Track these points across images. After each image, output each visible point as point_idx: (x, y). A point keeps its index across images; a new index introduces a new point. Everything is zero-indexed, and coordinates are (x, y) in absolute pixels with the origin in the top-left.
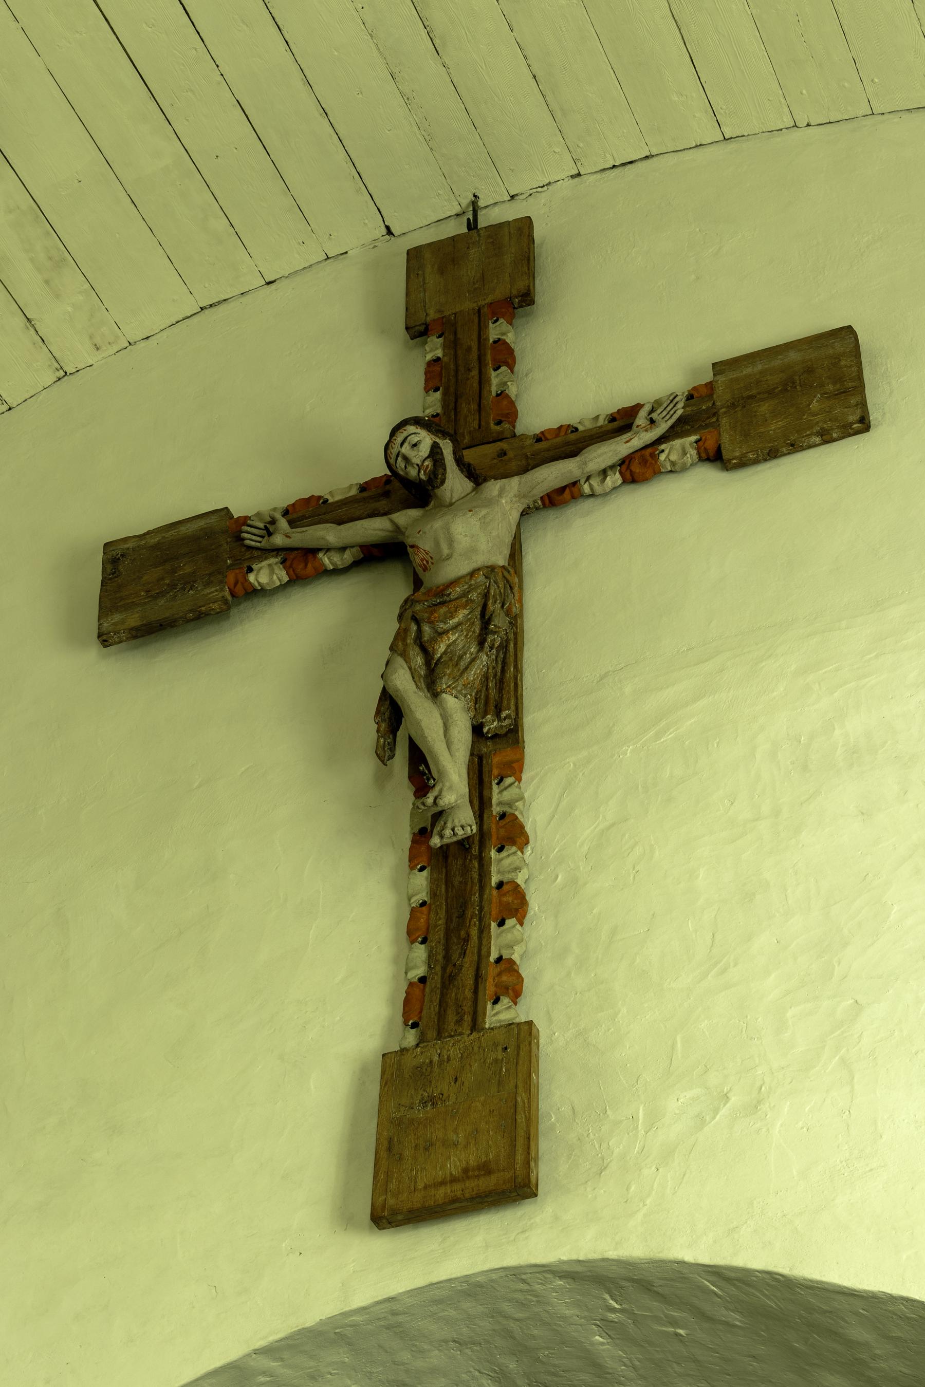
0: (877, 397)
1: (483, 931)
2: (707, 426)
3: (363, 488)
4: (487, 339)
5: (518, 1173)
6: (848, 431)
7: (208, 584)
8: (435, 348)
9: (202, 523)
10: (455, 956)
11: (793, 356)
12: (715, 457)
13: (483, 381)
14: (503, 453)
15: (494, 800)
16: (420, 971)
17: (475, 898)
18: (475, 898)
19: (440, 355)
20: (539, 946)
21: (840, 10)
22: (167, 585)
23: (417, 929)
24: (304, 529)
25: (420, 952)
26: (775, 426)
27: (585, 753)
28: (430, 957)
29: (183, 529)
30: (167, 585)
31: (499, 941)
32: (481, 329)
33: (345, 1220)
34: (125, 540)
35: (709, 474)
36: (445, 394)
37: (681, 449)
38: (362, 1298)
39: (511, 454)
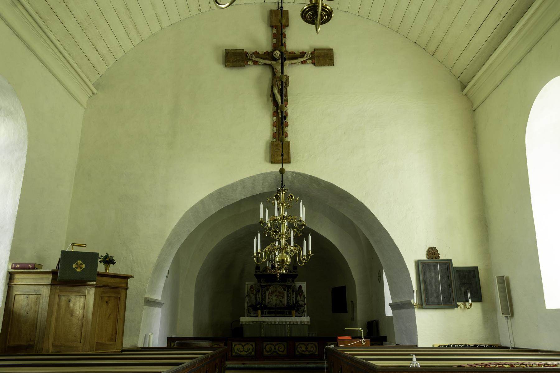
0: (336, 61)
3: (265, 53)
6: (331, 65)
11: (325, 51)
12: (314, 64)
16: (275, 131)
20: (289, 130)
21: (58, 83)
22: (235, 58)
23: (274, 125)
24: (76, 249)
25: (275, 128)
26: (322, 62)
27: (270, 283)
29: (238, 51)
30: (235, 58)
33: (266, 161)
35: (312, 66)
37: (309, 61)
38: (268, 171)
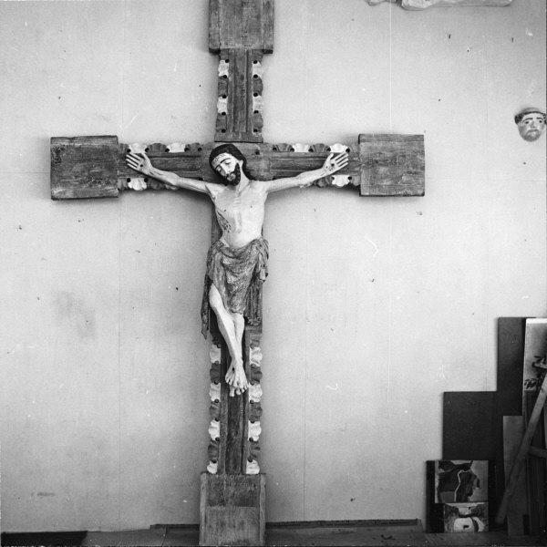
1: (245, 424)
2: (355, 172)
4: (251, 74)
5: (259, 210)
7: (108, 183)
8: (224, 69)
9: (104, 142)
10: (233, 434)
13: (249, 102)
14: (257, 153)
15: (250, 357)
17: (242, 406)
18: (242, 406)
19: (227, 74)
28: (221, 427)
31: (256, 103)
32: (249, 67)
34: (90, 138)
36: (230, 101)
39: (262, 154)
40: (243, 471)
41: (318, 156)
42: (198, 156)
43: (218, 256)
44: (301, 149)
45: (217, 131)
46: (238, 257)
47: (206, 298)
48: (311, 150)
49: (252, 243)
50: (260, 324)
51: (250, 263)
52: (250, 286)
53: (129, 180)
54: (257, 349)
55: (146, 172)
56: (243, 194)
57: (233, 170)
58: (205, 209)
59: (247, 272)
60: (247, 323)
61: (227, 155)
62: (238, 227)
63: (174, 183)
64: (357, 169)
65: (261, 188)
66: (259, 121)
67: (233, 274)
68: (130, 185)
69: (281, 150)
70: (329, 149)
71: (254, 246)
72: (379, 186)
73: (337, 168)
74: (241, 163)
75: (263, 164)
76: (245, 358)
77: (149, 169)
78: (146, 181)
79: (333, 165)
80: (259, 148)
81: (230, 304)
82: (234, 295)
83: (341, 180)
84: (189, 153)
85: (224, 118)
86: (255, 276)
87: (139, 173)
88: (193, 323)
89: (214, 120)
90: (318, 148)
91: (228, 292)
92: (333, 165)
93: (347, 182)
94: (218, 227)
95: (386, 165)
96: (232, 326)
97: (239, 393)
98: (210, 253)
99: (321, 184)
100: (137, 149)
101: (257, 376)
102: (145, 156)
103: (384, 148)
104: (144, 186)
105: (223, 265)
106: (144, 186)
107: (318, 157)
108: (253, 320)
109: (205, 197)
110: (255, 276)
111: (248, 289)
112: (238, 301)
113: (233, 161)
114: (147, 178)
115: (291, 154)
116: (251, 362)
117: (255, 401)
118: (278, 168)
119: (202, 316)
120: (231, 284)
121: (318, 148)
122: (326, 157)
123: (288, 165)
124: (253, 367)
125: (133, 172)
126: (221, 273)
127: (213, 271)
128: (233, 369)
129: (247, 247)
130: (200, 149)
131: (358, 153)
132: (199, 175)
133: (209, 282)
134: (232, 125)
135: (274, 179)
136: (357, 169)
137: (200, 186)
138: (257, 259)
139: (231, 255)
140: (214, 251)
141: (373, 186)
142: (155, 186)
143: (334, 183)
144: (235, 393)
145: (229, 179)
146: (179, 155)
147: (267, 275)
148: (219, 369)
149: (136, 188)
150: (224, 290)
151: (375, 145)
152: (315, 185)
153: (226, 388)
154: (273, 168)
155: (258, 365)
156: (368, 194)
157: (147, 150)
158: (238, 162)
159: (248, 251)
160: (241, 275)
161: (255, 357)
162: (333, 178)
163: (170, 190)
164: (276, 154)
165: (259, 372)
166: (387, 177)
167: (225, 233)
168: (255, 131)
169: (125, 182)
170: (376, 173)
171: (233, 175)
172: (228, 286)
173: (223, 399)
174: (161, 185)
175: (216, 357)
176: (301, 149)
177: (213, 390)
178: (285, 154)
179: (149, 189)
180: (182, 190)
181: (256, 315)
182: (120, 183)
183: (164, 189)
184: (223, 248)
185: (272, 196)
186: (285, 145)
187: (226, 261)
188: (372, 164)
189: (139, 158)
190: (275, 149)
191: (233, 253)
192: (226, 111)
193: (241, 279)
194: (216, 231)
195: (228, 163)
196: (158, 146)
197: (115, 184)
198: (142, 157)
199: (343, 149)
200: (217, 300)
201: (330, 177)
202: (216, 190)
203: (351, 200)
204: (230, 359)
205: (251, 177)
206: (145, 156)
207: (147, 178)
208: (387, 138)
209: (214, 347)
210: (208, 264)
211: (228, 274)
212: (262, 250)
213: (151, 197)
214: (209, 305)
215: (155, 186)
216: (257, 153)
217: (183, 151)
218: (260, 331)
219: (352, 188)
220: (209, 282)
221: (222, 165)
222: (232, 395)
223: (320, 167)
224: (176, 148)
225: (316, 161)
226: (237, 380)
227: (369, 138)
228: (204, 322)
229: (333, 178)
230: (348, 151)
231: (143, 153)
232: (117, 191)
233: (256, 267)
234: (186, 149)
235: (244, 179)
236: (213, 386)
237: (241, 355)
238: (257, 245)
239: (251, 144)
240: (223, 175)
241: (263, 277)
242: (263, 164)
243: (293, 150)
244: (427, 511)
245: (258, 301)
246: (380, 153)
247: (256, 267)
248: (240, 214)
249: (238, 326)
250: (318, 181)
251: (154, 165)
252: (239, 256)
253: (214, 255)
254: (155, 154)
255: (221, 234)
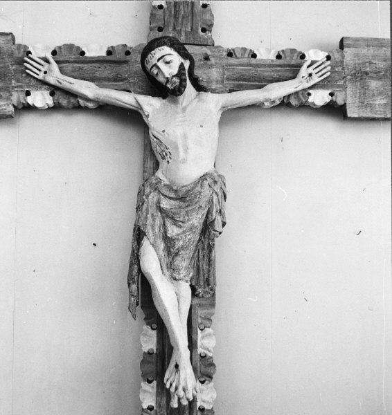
2: (339, 86)
14: (207, 58)
15: (199, 344)
39: (213, 61)
40: (177, 408)
41: (289, 65)
42: (126, 62)
43: (153, 198)
44: (266, 54)
45: (151, 29)
46: (182, 199)
47: (136, 258)
48: (279, 57)
49: (203, 178)
50: (214, 295)
51: (200, 207)
52: (200, 239)
53: (28, 94)
54: (208, 330)
55: (52, 80)
56: (188, 110)
57: (175, 72)
58: (130, 136)
59: (197, 220)
60: (194, 293)
61: (166, 50)
62: (182, 154)
63: (90, 95)
64: (341, 83)
65: (214, 103)
66: (207, 17)
67: (175, 222)
68: (30, 100)
69: (238, 56)
70: (303, 57)
71: (206, 183)
72: (370, 105)
73: (316, 79)
74: (187, 64)
75: (215, 73)
76: (192, 345)
77: (55, 75)
78: (52, 94)
79: (310, 75)
80: (209, 52)
81: (170, 268)
82: (177, 254)
83: (320, 98)
84: (111, 58)
85: (160, 12)
86: (207, 228)
87: (44, 83)
88: (118, 291)
89: (148, 15)
90: (288, 54)
91: (168, 249)
92: (310, 75)
93: (328, 99)
94: (153, 155)
95: (379, 79)
96: (173, 299)
97: (185, 403)
98: (141, 193)
99: (293, 102)
100: (40, 50)
101: (210, 370)
102: (52, 60)
103: (374, 56)
104: (50, 101)
105: (161, 210)
106: (50, 101)
107: (289, 66)
108: (203, 287)
109: (133, 117)
110: (207, 228)
111: (197, 246)
112: (183, 263)
113: (176, 59)
114: (54, 90)
115: (253, 61)
116: (200, 350)
117: (207, 407)
118: (234, 80)
119: (129, 284)
120: (179, 228)
121: (288, 54)
122: (300, 66)
123: (247, 73)
124: (203, 357)
125: (33, 82)
126: (158, 222)
127: (146, 218)
128: (177, 366)
129: (196, 184)
130: (128, 53)
131: (342, 62)
132: (126, 86)
133: (139, 235)
134: (172, 20)
135: (230, 91)
136: (341, 83)
137: (126, 99)
138: (211, 202)
139: (173, 195)
140: (147, 190)
141: (362, 105)
142: (64, 102)
143: (311, 99)
144: (179, 403)
145: (169, 86)
146: (98, 60)
147: (224, 224)
148: (154, 360)
149: (39, 104)
150: (162, 246)
151: (364, 51)
152: (284, 104)
153: (164, 392)
154: (227, 79)
155: (210, 354)
156: (356, 115)
157: (54, 53)
158: (183, 61)
159: (198, 189)
160: (187, 225)
161: (206, 342)
162: (309, 94)
163: (85, 109)
164: (232, 61)
165: (212, 365)
166: (380, 94)
167: (163, 163)
168: (204, 30)
169: (22, 95)
170: (365, 88)
171: (176, 80)
172: (168, 241)
173: (159, 404)
174: (73, 100)
175: (150, 343)
176: (266, 54)
177: (145, 391)
178: (245, 61)
179: (57, 108)
180: (105, 109)
181: (207, 282)
182: (16, 97)
183: (78, 108)
184: (160, 186)
185: (230, 115)
186: (245, 49)
187: (166, 204)
188: (361, 75)
189: (42, 62)
190: (230, 54)
191: (176, 191)
192: (153, 404)
193: (186, 233)
194: (150, 164)
195: (168, 63)
196: (70, 47)
197: (8, 99)
198: (47, 61)
199: (321, 56)
200: (152, 261)
201: (306, 92)
202: (151, 105)
203: (328, 128)
204: (171, 349)
205: (199, 88)
206: (52, 60)
207: (54, 90)
208: (165, 310)
209: (146, 328)
210: (138, 208)
211: (168, 223)
212: (217, 188)
213: (59, 119)
214: (140, 270)
215: (66, 102)
216: (207, 58)
217: (104, 54)
218: (213, 305)
219: (335, 110)
220: (139, 235)
221: (160, 64)
222: (175, 405)
223: (294, 77)
224: (95, 50)
225: (286, 71)
226: (182, 384)
227: (357, 42)
228: (131, 294)
229: (309, 94)
230: (328, 58)
231: (49, 56)
232: (11, 109)
233: (209, 212)
234: (109, 53)
235: (190, 89)
236: (145, 386)
237: (187, 343)
238: (209, 180)
239: (197, 47)
240: (161, 79)
241: (218, 226)
242: (215, 73)
243: (254, 56)
244: (167, 325)
245: (210, 262)
246: (370, 63)
247: (209, 212)
248: (185, 137)
249: (182, 300)
250: (289, 96)
251: (62, 71)
252: (184, 197)
253: (147, 196)
254: (66, 58)
255: (157, 165)
